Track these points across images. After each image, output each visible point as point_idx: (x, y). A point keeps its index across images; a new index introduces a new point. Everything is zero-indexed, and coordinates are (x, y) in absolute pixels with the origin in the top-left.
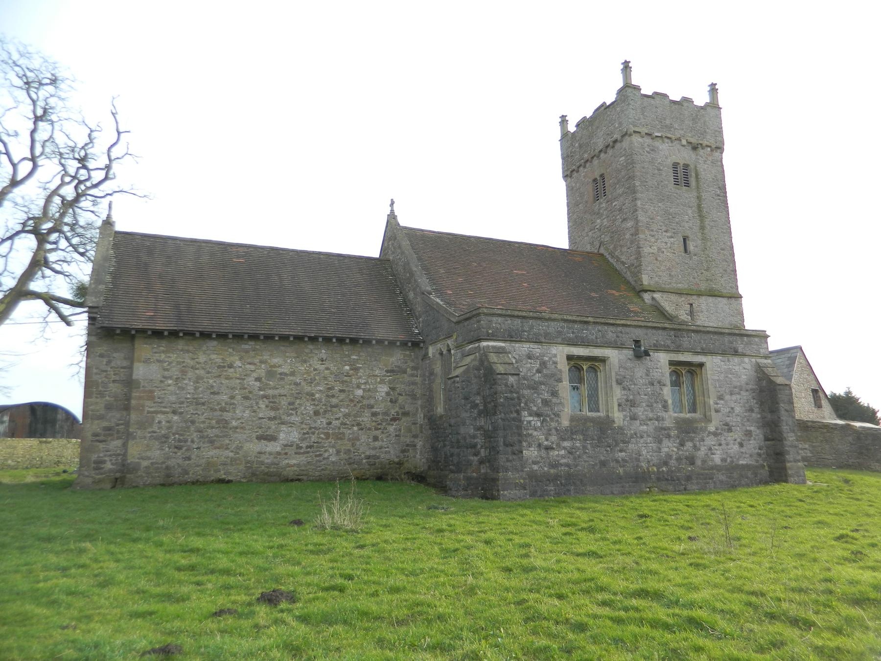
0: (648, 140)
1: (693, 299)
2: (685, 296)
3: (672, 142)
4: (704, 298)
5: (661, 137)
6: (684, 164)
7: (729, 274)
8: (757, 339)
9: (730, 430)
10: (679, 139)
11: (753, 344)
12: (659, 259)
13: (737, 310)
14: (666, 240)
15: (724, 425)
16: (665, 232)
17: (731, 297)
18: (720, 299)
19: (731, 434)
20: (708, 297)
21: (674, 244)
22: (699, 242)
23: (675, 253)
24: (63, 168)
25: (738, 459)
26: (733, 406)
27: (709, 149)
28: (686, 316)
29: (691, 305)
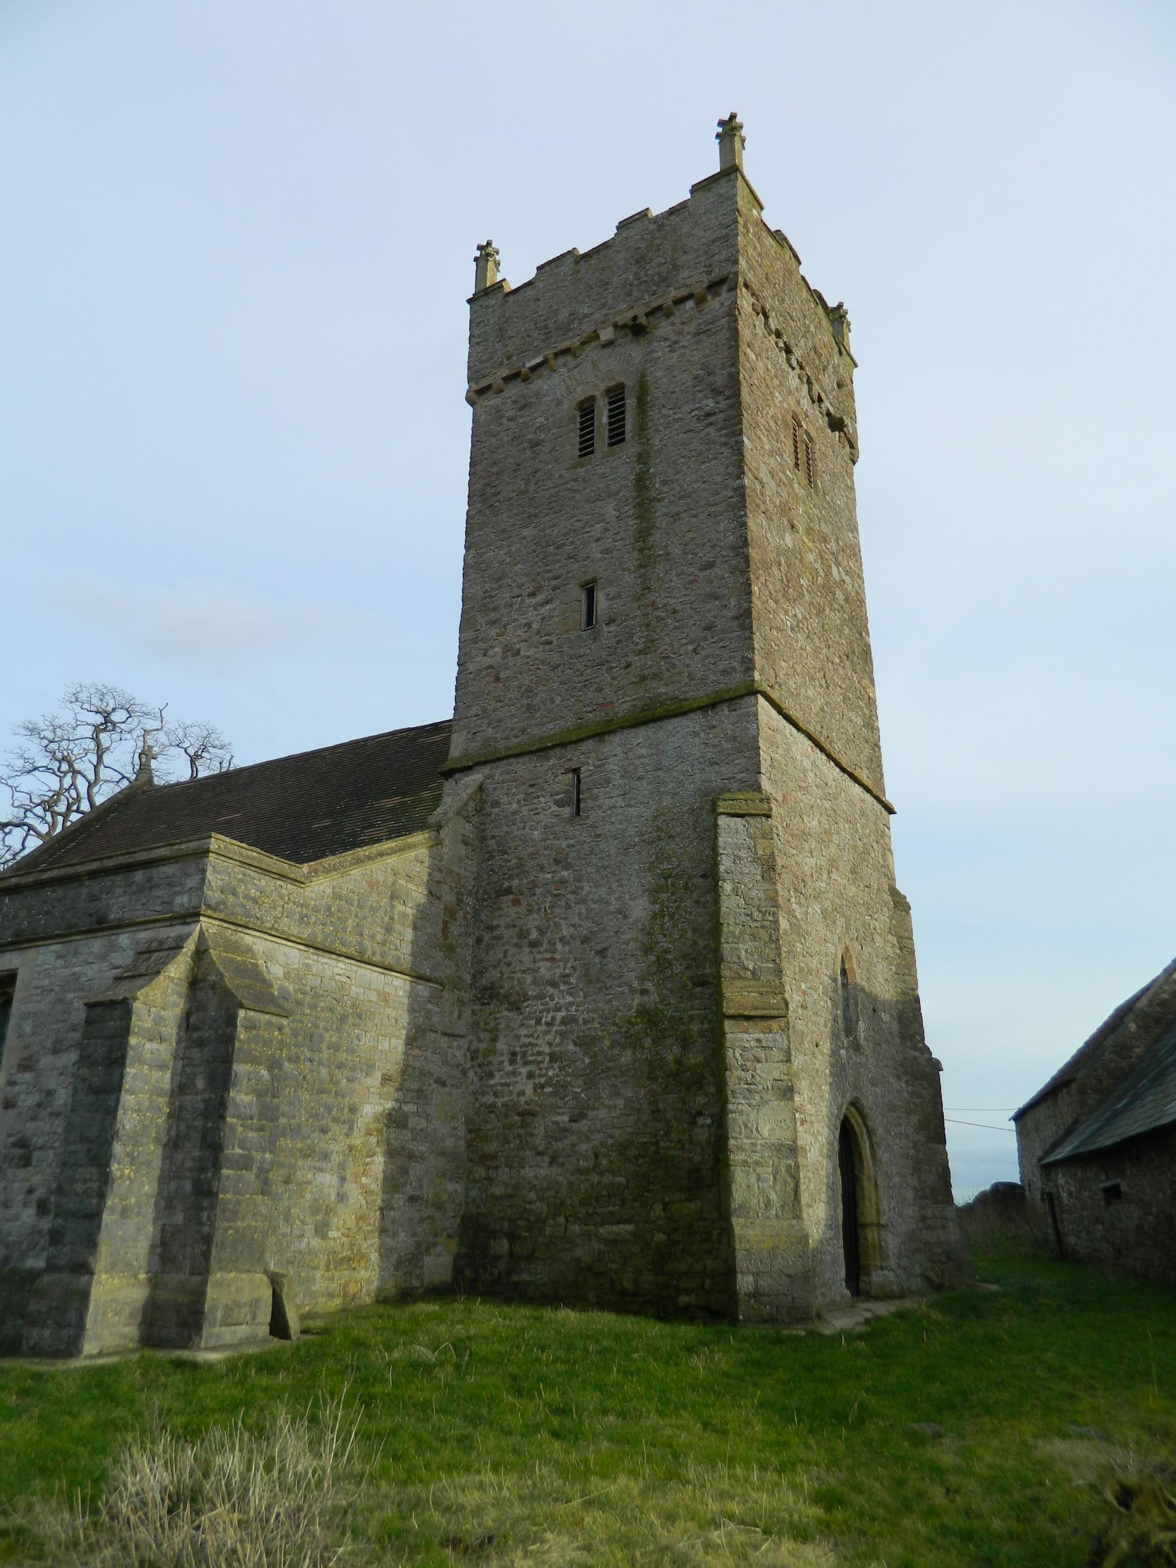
0: (514, 390)
1: (575, 755)
2: (558, 751)
3: (575, 357)
4: (616, 739)
5: (545, 362)
6: (609, 391)
7: (724, 631)
8: (170, 870)
9: (26, 1161)
10: (595, 336)
11: (157, 886)
12: (504, 675)
13: (734, 739)
14: (532, 615)
15: (14, 1145)
16: (529, 596)
17: (712, 706)
18: (670, 725)
19: (22, 1173)
20: (633, 732)
21: (551, 617)
22: (629, 578)
23: (551, 643)
24: (26, 828)
25: (24, 1255)
26: (53, 1087)
27: (690, 304)
28: (554, 808)
29: (576, 771)
